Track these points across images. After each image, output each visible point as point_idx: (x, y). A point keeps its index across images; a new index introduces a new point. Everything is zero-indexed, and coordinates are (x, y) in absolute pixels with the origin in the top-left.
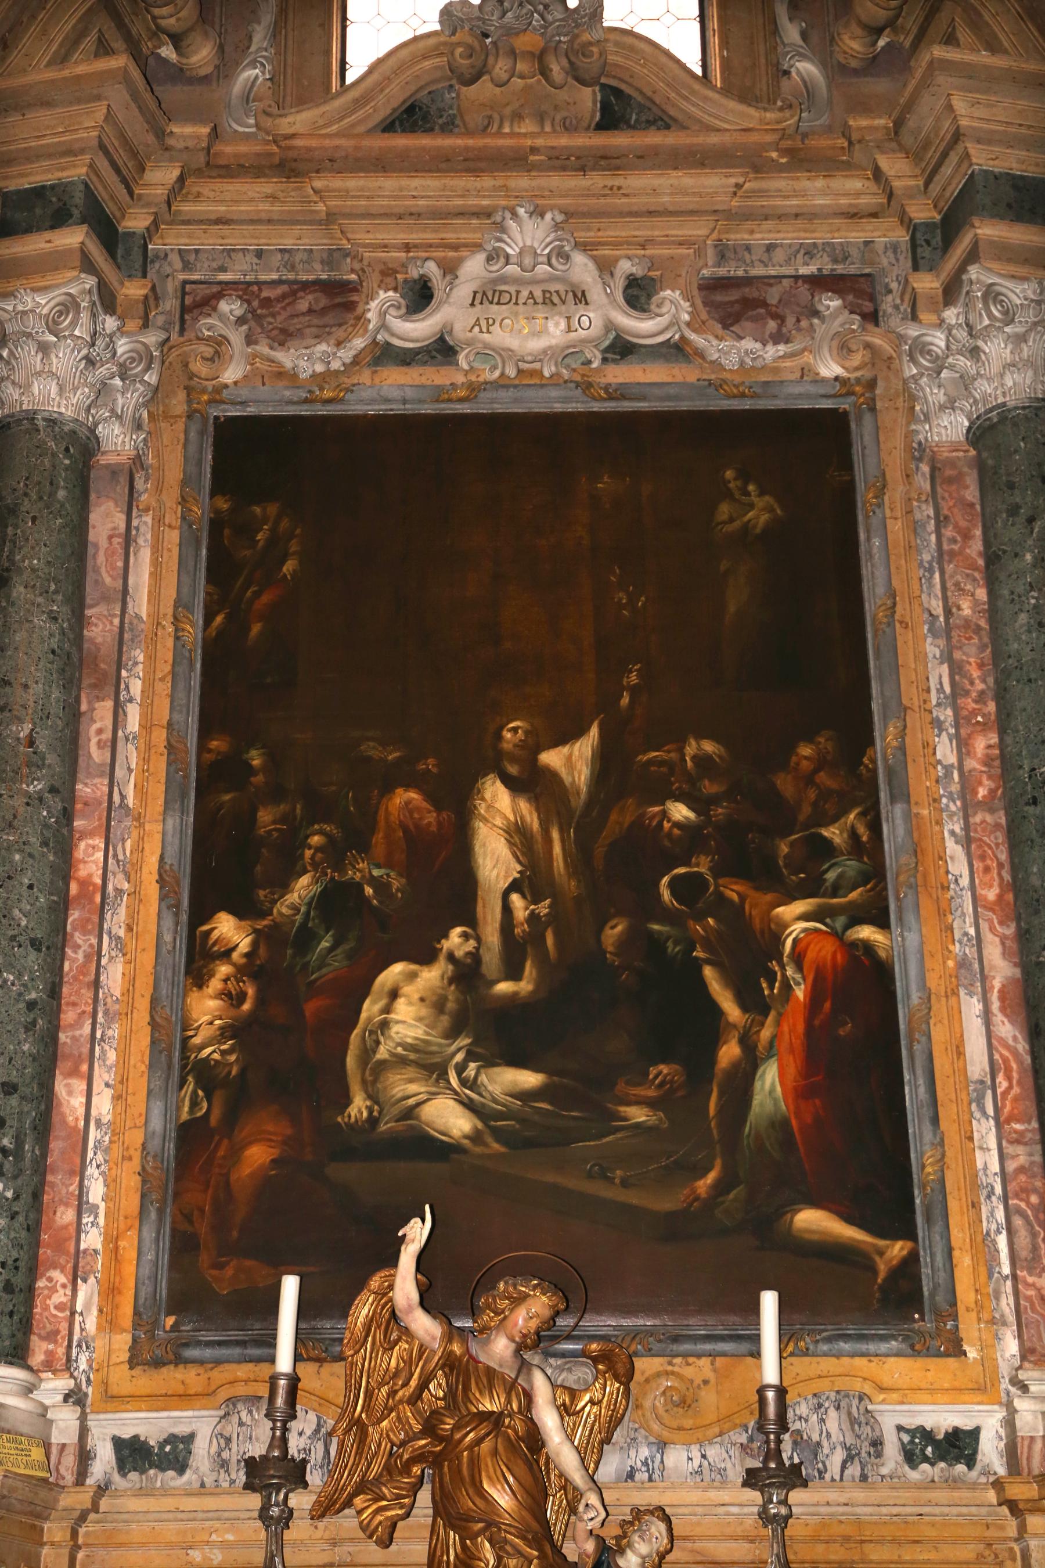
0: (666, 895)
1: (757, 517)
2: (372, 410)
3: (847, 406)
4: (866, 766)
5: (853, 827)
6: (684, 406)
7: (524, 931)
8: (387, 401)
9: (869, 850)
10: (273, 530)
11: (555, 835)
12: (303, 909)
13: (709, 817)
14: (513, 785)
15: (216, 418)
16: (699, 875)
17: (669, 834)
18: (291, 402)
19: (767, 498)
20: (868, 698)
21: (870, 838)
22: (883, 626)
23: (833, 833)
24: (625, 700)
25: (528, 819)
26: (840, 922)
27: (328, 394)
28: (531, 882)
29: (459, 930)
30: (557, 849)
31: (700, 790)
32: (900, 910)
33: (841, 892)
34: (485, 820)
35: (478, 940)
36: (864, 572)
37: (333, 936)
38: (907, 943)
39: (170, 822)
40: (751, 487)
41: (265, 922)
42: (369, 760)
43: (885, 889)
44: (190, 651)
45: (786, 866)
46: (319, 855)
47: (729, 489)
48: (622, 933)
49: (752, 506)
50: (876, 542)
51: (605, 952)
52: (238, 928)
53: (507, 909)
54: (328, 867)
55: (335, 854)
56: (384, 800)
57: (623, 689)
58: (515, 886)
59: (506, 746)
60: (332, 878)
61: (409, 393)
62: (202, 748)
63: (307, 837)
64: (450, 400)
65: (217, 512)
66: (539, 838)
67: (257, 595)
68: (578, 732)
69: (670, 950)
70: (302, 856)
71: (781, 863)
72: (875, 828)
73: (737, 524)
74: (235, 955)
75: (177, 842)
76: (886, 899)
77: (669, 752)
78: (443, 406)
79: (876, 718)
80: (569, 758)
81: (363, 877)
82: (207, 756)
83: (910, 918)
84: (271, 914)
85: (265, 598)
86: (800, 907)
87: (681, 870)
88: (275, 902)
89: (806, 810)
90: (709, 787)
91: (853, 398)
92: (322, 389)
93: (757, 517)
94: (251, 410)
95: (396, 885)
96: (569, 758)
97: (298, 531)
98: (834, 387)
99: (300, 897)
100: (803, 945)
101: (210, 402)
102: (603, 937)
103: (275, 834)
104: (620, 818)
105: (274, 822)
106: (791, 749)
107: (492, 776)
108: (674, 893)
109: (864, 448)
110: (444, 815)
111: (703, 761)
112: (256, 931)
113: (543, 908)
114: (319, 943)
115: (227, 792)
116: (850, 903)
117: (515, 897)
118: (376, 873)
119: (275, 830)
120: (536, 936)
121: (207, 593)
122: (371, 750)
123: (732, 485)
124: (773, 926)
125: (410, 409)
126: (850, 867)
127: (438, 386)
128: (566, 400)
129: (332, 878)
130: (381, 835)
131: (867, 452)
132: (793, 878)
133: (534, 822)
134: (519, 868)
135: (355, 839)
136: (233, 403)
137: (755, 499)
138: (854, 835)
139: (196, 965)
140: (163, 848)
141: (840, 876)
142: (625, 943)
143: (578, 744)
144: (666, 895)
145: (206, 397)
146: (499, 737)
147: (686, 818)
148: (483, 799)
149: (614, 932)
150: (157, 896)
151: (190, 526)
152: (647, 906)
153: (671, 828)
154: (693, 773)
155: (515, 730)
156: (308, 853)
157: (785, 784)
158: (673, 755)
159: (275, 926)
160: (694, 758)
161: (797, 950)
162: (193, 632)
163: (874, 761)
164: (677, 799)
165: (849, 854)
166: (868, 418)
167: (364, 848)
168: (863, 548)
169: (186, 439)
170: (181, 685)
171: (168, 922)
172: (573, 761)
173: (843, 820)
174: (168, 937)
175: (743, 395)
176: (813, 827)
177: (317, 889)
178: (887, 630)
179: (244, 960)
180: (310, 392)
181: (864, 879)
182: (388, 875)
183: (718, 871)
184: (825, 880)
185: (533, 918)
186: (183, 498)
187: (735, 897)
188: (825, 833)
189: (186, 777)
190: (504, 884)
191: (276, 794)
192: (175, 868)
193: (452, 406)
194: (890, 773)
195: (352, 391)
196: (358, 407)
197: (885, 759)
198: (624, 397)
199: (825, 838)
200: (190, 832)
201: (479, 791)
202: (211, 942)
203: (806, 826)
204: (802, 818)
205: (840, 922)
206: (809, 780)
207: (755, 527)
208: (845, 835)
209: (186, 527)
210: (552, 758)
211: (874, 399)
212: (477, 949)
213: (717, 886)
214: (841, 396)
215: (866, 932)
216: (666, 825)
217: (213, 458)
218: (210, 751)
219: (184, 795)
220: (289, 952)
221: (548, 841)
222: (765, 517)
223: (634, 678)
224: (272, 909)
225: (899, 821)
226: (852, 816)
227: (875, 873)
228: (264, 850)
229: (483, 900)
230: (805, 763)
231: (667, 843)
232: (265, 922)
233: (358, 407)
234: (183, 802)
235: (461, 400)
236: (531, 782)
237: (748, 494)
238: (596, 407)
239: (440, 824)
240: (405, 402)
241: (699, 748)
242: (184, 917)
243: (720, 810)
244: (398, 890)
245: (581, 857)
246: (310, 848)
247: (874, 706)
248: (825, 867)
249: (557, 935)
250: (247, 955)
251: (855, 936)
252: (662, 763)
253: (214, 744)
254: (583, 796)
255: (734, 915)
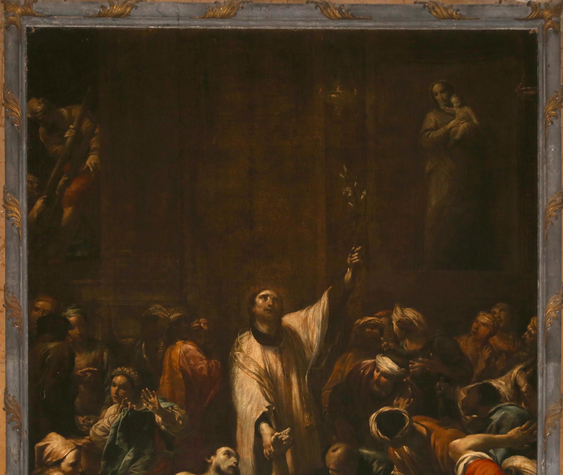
0: (374, 427)
1: (457, 125)
2: (153, 24)
3: (536, 29)
4: (530, 332)
5: (515, 379)
6: (403, 26)
7: (270, 451)
8: (165, 16)
9: (526, 397)
10: (78, 129)
11: (294, 380)
12: (111, 431)
13: (408, 369)
14: (264, 341)
15: (29, 29)
16: (398, 413)
17: (378, 381)
18: (87, 16)
19: (466, 109)
20: (535, 278)
21: (528, 389)
22: (552, 219)
23: (501, 384)
24: (348, 276)
25: (274, 367)
26: (501, 452)
27: (117, 10)
28: (275, 415)
29: (223, 449)
30: (295, 391)
31: (402, 348)
32: (545, 445)
33: (503, 430)
34: (243, 367)
35: (238, 457)
36: (540, 173)
37: (133, 451)
38: (549, 471)
39: (11, 364)
40: (454, 100)
41: (84, 441)
42: (157, 318)
43: (536, 428)
44: (18, 229)
45: (463, 409)
46: (122, 391)
47: (436, 101)
48: (341, 455)
49: (453, 116)
50: (552, 148)
51: (328, 469)
52: (65, 445)
53: (258, 435)
54: (128, 400)
55: (133, 391)
56: (169, 350)
57: (347, 266)
58: (264, 418)
59: (259, 310)
60: (132, 409)
61: (183, 10)
62: (31, 307)
63: (112, 377)
64: (214, 17)
65: (33, 112)
66: (282, 381)
67: (68, 183)
68: (313, 300)
69: (375, 469)
70: (109, 391)
71: (459, 406)
72: (533, 381)
73: (442, 130)
74: (63, 465)
75: (17, 379)
76: (536, 436)
77: (380, 317)
78: (209, 22)
79: (540, 294)
80: (305, 320)
81: (154, 408)
82: (36, 314)
83: (552, 451)
84: (88, 435)
85: (74, 187)
86: (472, 440)
87: (386, 409)
88: (90, 426)
89: (482, 365)
90: (409, 346)
91: (542, 22)
92: (112, 5)
93: (457, 125)
94: (56, 23)
95: (178, 414)
96: (305, 320)
97: (97, 131)
98: (527, 11)
99: (109, 422)
100: (471, 469)
101: (25, 14)
102: (327, 457)
103: (89, 375)
104: (342, 368)
105: (88, 365)
106: (472, 316)
107: (247, 333)
108: (379, 427)
109: (548, 66)
110: (213, 362)
111: (405, 325)
112: (77, 447)
113: (284, 435)
114: (124, 457)
115: (52, 341)
116: (509, 438)
117: (264, 426)
118: (163, 405)
119: (88, 371)
120: (279, 456)
121: (29, 182)
122: (157, 310)
123: (438, 97)
124: (450, 454)
125: (183, 24)
126: (510, 410)
127: (205, 4)
128: (307, 19)
129: (132, 409)
130: (166, 376)
131: (550, 69)
132: (468, 417)
133: (278, 369)
134: (267, 404)
135: (147, 378)
136: (42, 16)
137: (457, 110)
138: (516, 386)
139: (35, 472)
140: (6, 384)
141: (503, 418)
142: (343, 462)
143: (312, 309)
144: (374, 427)
145: (19, 10)
146: (253, 303)
147: (391, 369)
148: (241, 351)
149: (336, 453)
150: (4, 420)
151: (13, 124)
152: (360, 435)
153: (379, 376)
154: (397, 334)
155: (265, 297)
156: (114, 389)
157: (467, 344)
158: (383, 319)
159: (92, 444)
160: (398, 322)
161: (467, 472)
162: (20, 214)
163: (535, 328)
164: (385, 354)
165: (511, 400)
166: (553, 39)
167: (154, 387)
168: (540, 153)
169: (6, 48)
170: (13, 256)
171: (14, 440)
172: (308, 323)
173: (508, 374)
174: (14, 451)
175: (451, 17)
176: (486, 379)
177: (121, 416)
178: (555, 222)
179: (70, 469)
180: (102, 7)
181: (521, 420)
182: (172, 407)
183: (413, 411)
184: (491, 420)
185: (277, 442)
186: (5, 99)
187: (424, 431)
188: (494, 384)
189: (21, 329)
190: (256, 416)
191: (89, 343)
192: (17, 398)
193: (216, 22)
194: (548, 338)
195: (136, 7)
196: (142, 22)
197: (545, 327)
198: (354, 17)
199: (493, 388)
200: (26, 372)
201: (238, 344)
202: (46, 455)
203: (479, 379)
204: (477, 371)
205: (501, 452)
206: (485, 341)
207: (455, 133)
208: (509, 386)
209: (9, 126)
210: (292, 320)
211: (558, 23)
212: (237, 464)
213: (411, 421)
214: (532, 19)
215: (518, 461)
216: (376, 374)
217: (28, 65)
218: (37, 309)
219: (20, 344)
220: (102, 463)
221: (289, 384)
222: (463, 126)
223: (355, 258)
224: (88, 432)
225: (551, 377)
226: (515, 371)
227: (529, 417)
228: (81, 387)
229: (240, 426)
230: (483, 329)
231: (376, 389)
232: (84, 441)
233: (142, 22)
234: (19, 350)
235: (223, 17)
236: (276, 338)
237: (450, 105)
238: (332, 26)
239: (209, 370)
240: (178, 18)
241: (403, 315)
242: (26, 436)
243: (416, 364)
244: (180, 418)
245: (312, 397)
246: (115, 386)
247: (540, 285)
248: (492, 410)
249: (294, 455)
250: (72, 465)
251: (510, 464)
252: (374, 326)
253: (40, 304)
254: (315, 350)
255: (423, 444)
